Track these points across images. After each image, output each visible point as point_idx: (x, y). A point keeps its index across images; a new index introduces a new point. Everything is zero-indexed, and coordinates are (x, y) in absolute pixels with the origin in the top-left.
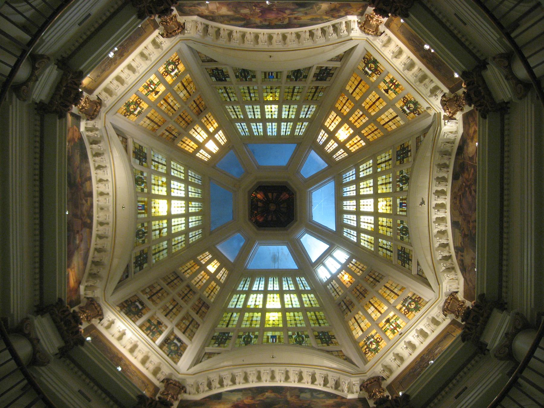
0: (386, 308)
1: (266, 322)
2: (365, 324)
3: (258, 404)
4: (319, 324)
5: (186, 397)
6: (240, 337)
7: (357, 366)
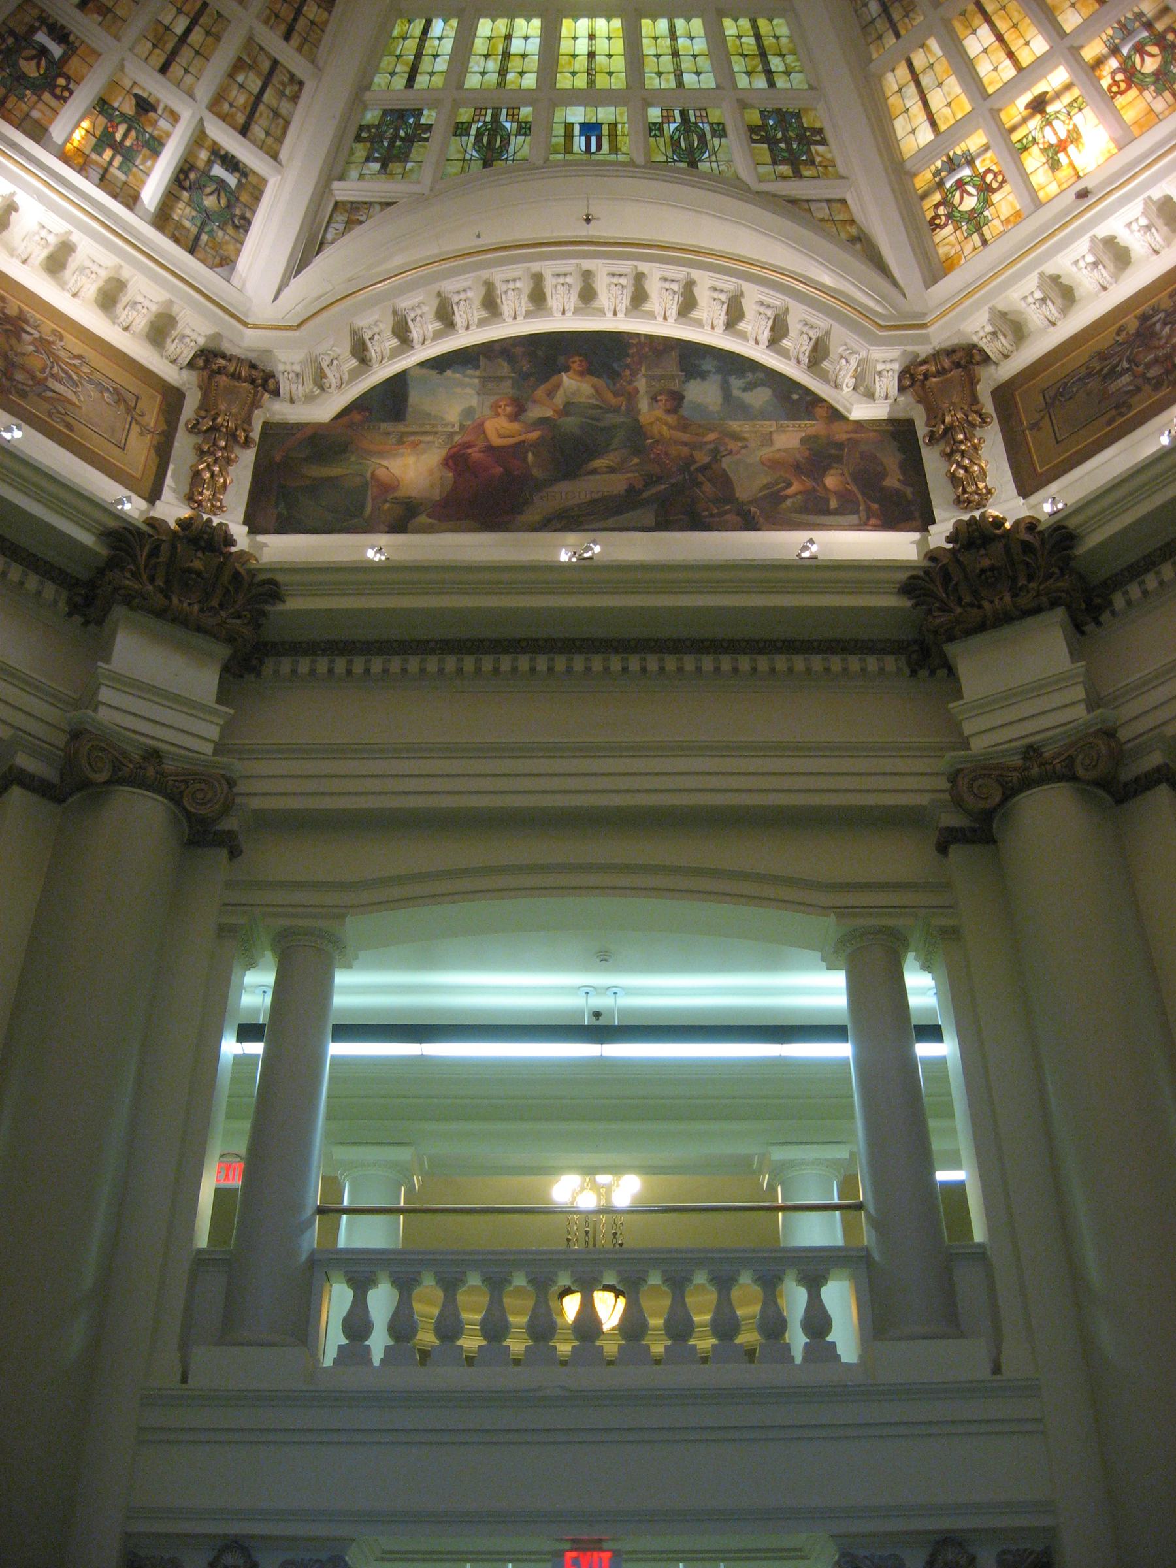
0: (1040, 45)
1: (563, 60)
2: (949, 98)
3: (535, 445)
4: (769, 73)
5: (281, 411)
6: (461, 129)
7: (895, 284)
